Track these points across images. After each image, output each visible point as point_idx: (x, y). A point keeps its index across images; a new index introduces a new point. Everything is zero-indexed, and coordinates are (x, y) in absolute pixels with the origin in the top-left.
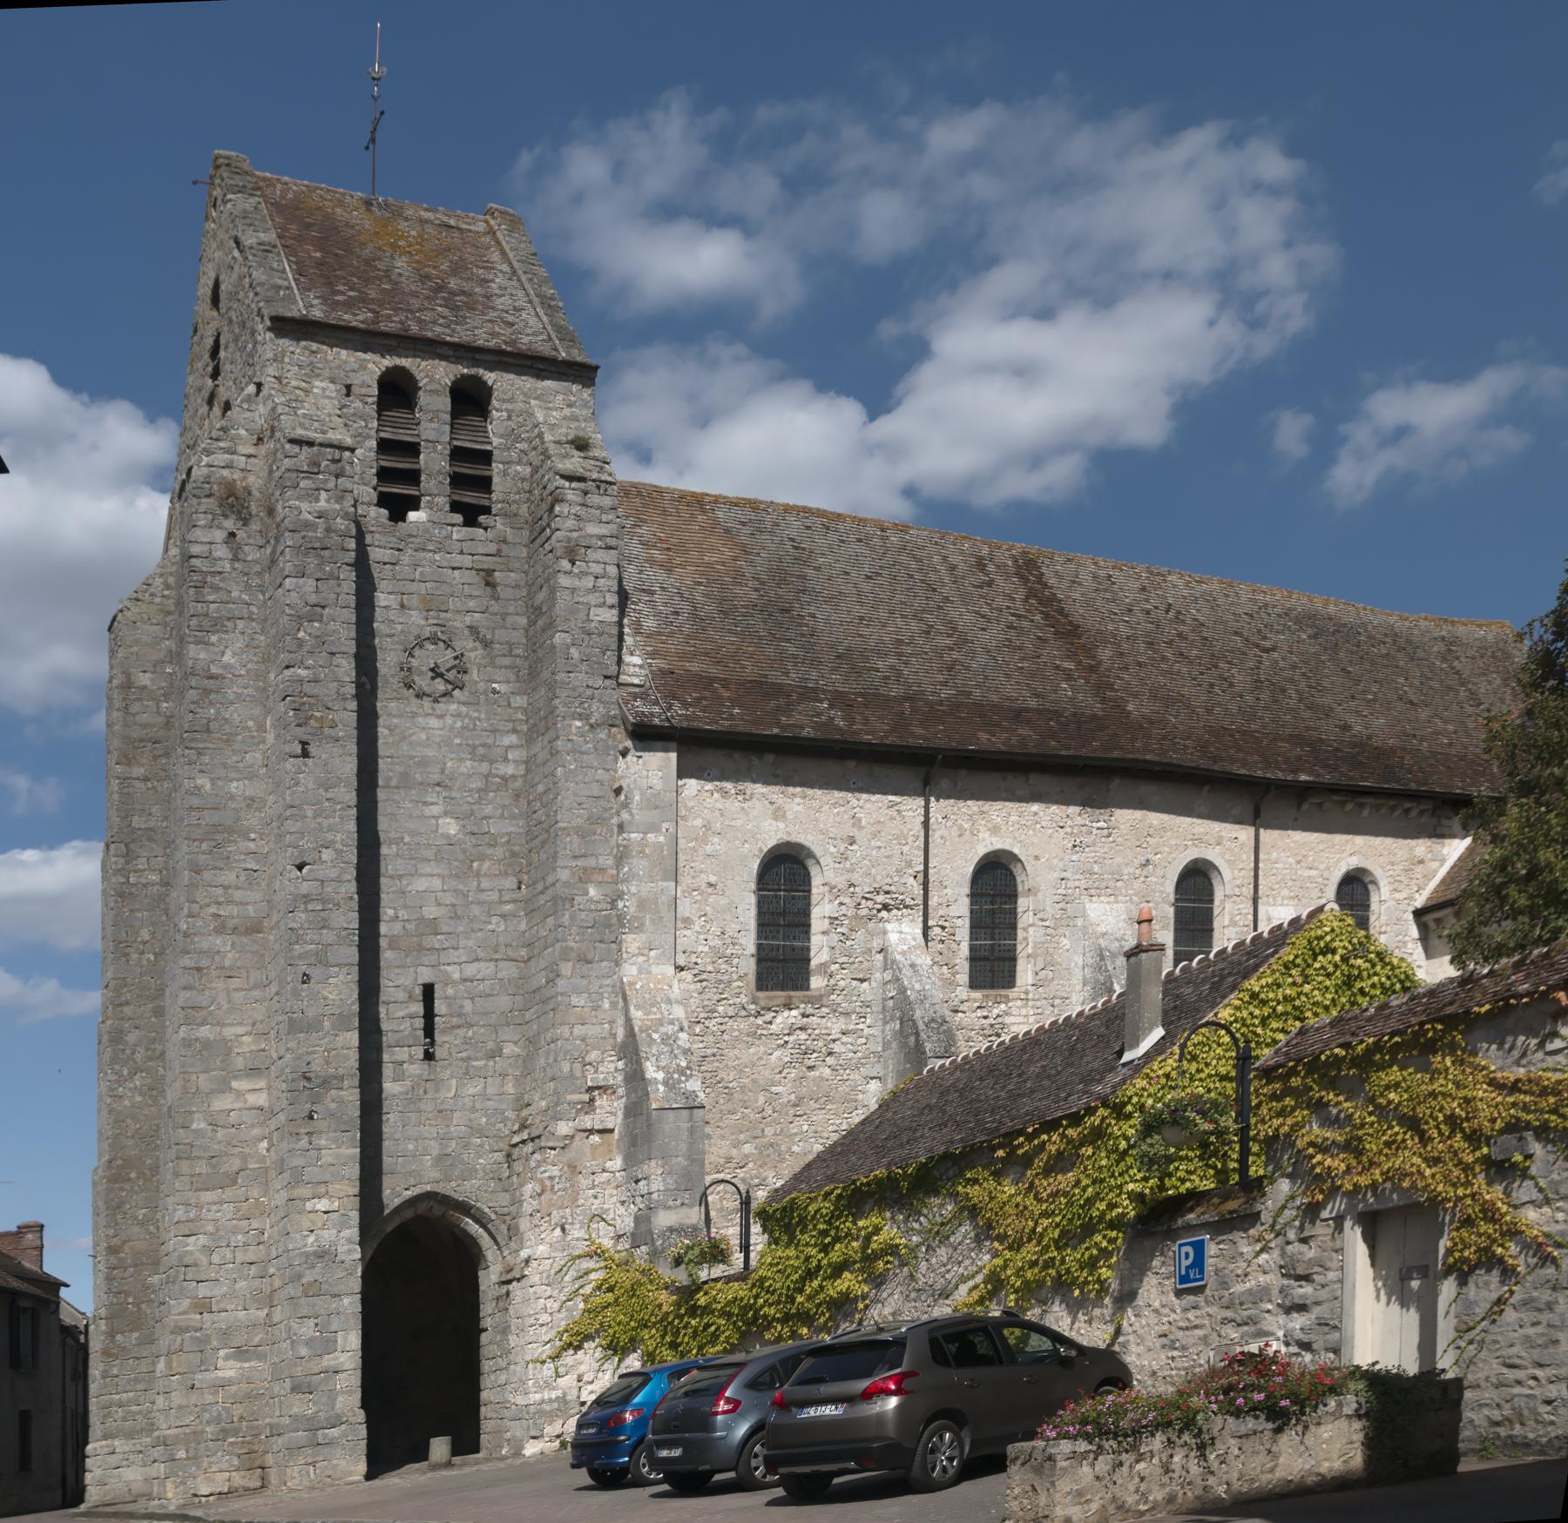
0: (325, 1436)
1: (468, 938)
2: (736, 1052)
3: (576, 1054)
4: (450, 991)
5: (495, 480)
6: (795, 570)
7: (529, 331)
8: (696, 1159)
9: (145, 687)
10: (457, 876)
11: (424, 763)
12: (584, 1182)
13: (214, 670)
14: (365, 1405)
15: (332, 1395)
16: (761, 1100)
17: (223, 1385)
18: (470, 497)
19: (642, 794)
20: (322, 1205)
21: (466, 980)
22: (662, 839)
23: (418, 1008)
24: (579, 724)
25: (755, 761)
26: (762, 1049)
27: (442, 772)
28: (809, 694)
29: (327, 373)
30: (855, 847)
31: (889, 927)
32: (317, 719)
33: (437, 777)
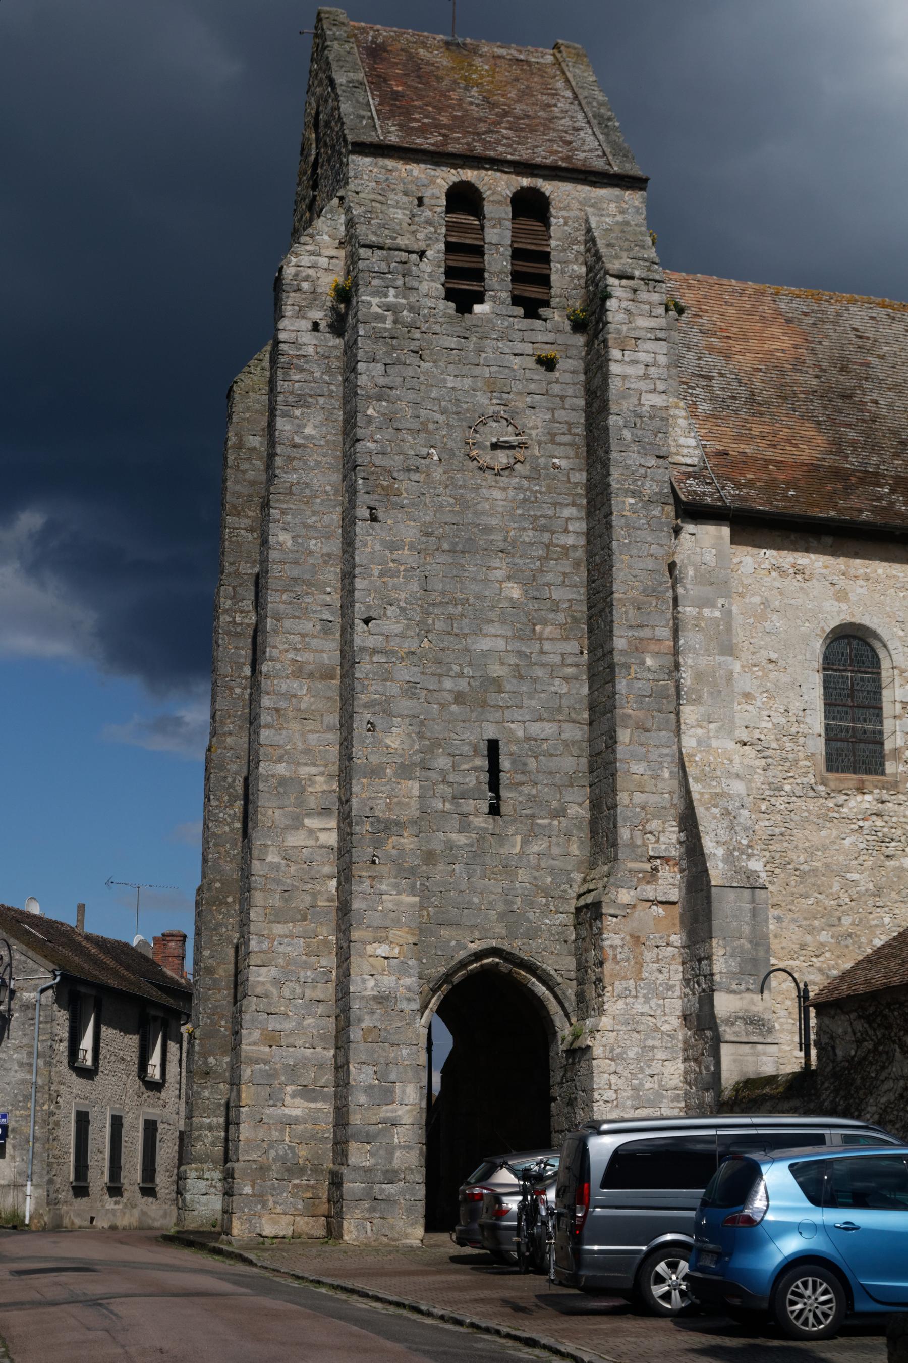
0: (382, 1191)
1: (531, 698)
2: (807, 833)
3: (636, 822)
4: (514, 748)
5: (553, 277)
6: (858, 358)
7: (586, 148)
8: (760, 941)
9: (255, 448)
11: (488, 530)
12: (648, 955)
13: (297, 440)
15: (390, 1150)
17: (290, 1122)
18: (532, 291)
19: (697, 570)
21: (528, 739)
22: (717, 614)
24: (632, 501)
25: (814, 543)
26: (835, 833)
27: (505, 540)
28: (872, 478)
32: (383, 487)
33: (501, 545)
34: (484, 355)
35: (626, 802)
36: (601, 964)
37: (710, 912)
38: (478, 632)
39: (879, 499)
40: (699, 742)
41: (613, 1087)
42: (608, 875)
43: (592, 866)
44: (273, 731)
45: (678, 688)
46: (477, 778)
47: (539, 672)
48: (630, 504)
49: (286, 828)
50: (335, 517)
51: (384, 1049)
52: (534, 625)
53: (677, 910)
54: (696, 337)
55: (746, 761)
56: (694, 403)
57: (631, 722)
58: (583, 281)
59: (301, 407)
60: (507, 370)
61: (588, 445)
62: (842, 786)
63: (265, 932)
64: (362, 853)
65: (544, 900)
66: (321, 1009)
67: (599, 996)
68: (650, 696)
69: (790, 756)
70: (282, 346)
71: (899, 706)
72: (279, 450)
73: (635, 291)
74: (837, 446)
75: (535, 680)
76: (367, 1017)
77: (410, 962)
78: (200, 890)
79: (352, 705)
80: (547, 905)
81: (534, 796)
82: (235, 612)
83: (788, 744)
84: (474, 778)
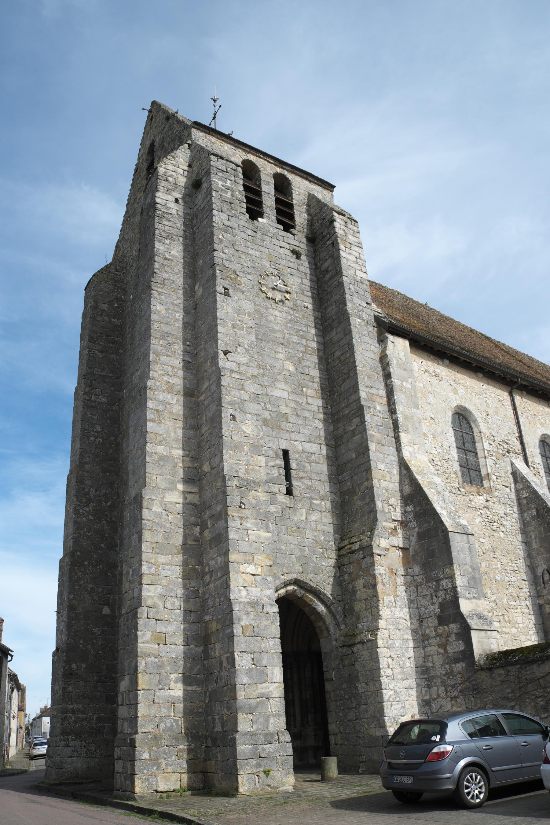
0: (264, 750)
10: (295, 393)
11: (274, 331)
13: (167, 256)
19: (397, 361)
20: (251, 569)
21: (304, 452)
22: (409, 386)
23: (281, 462)
24: (360, 321)
30: (489, 417)
34: (265, 243)
35: (378, 486)
38: (273, 385)
41: (391, 667)
44: (155, 424)
46: (279, 471)
47: (307, 414)
48: (359, 322)
51: (257, 641)
52: (302, 387)
59: (169, 239)
60: (277, 253)
62: (471, 490)
63: (153, 561)
65: (321, 550)
68: (382, 426)
70: (157, 205)
75: (305, 418)
76: (244, 617)
77: (269, 578)
80: (323, 553)
81: (310, 486)
82: (92, 394)
83: (445, 464)
84: (277, 472)
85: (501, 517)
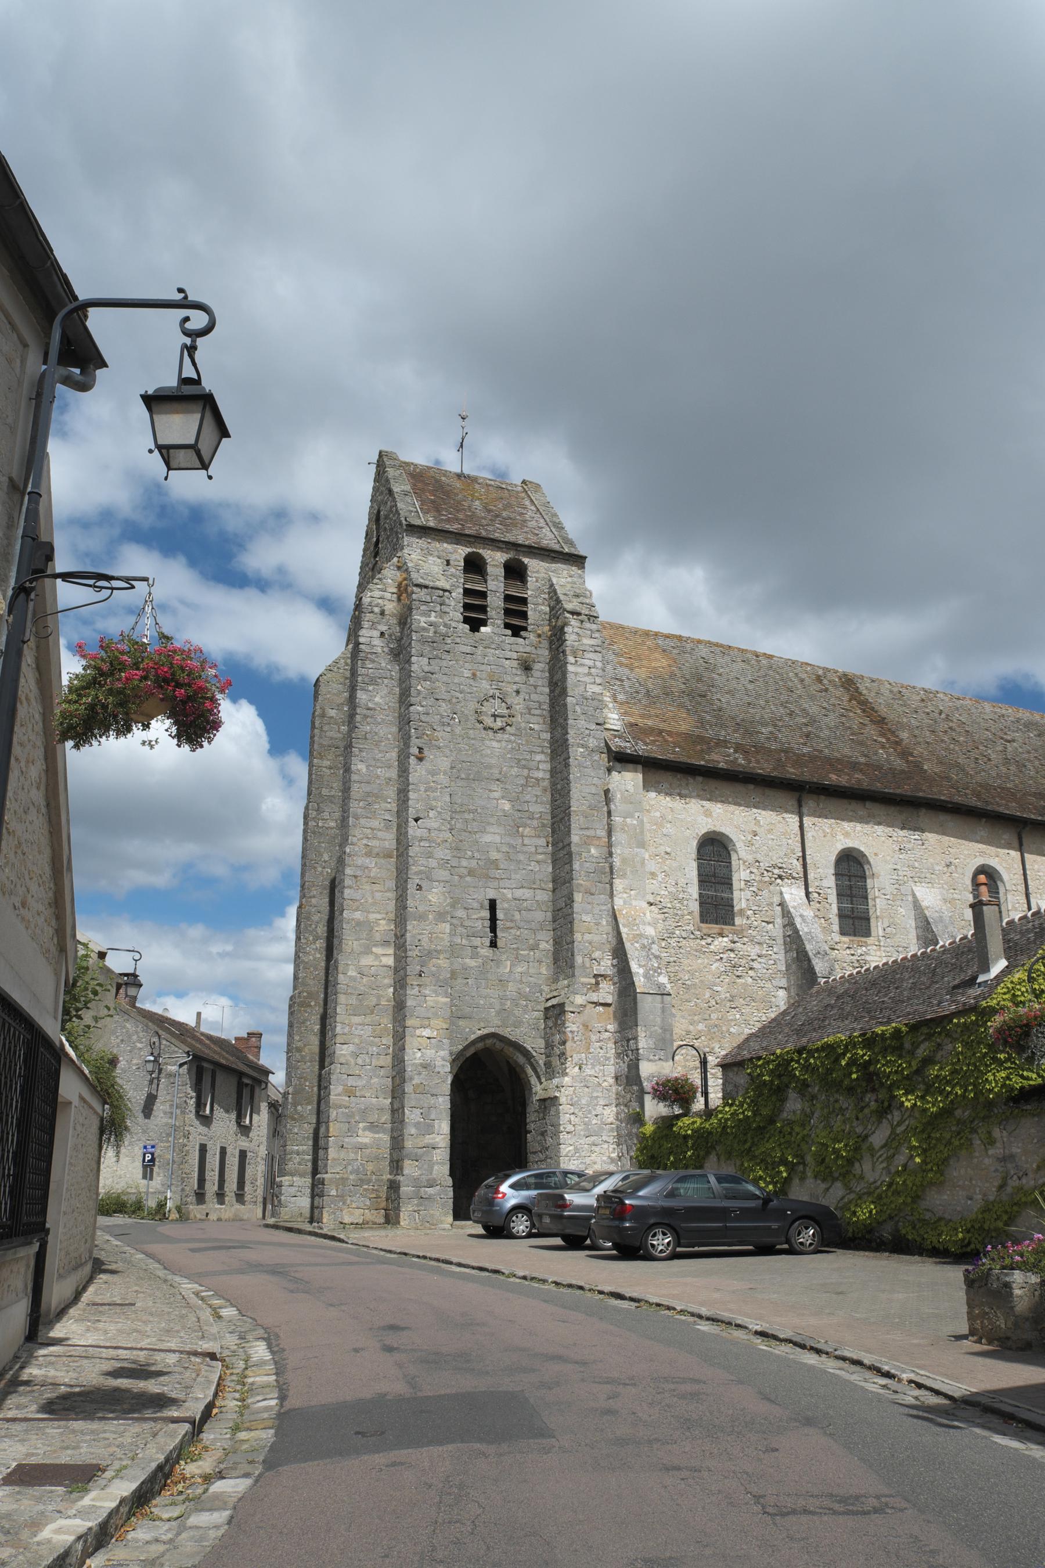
0: (426, 1193)
4: (506, 905)
5: (529, 613)
8: (667, 1029)
10: (509, 835)
11: (489, 767)
12: (594, 1038)
13: (370, 705)
14: (452, 1174)
16: (707, 995)
17: (361, 1148)
19: (622, 794)
20: (427, 1033)
22: (635, 822)
23: (486, 914)
28: (723, 743)
29: (436, 553)
30: (757, 838)
31: (784, 890)
33: (498, 776)
36: (564, 1043)
37: (636, 1009)
39: (729, 756)
40: (625, 903)
42: (568, 986)
43: (556, 980)
45: (611, 867)
47: (521, 857)
49: (361, 953)
50: (394, 755)
53: (611, 1009)
54: (612, 657)
55: (653, 915)
56: (615, 695)
57: (582, 889)
58: (547, 617)
61: (551, 716)
64: (413, 969)
66: (382, 1072)
67: (562, 1064)
69: (679, 912)
70: (361, 646)
71: (743, 883)
72: (358, 711)
73: (582, 622)
74: (702, 723)
78: (291, 999)
79: (407, 874)
80: (526, 1006)
85: (753, 960)
